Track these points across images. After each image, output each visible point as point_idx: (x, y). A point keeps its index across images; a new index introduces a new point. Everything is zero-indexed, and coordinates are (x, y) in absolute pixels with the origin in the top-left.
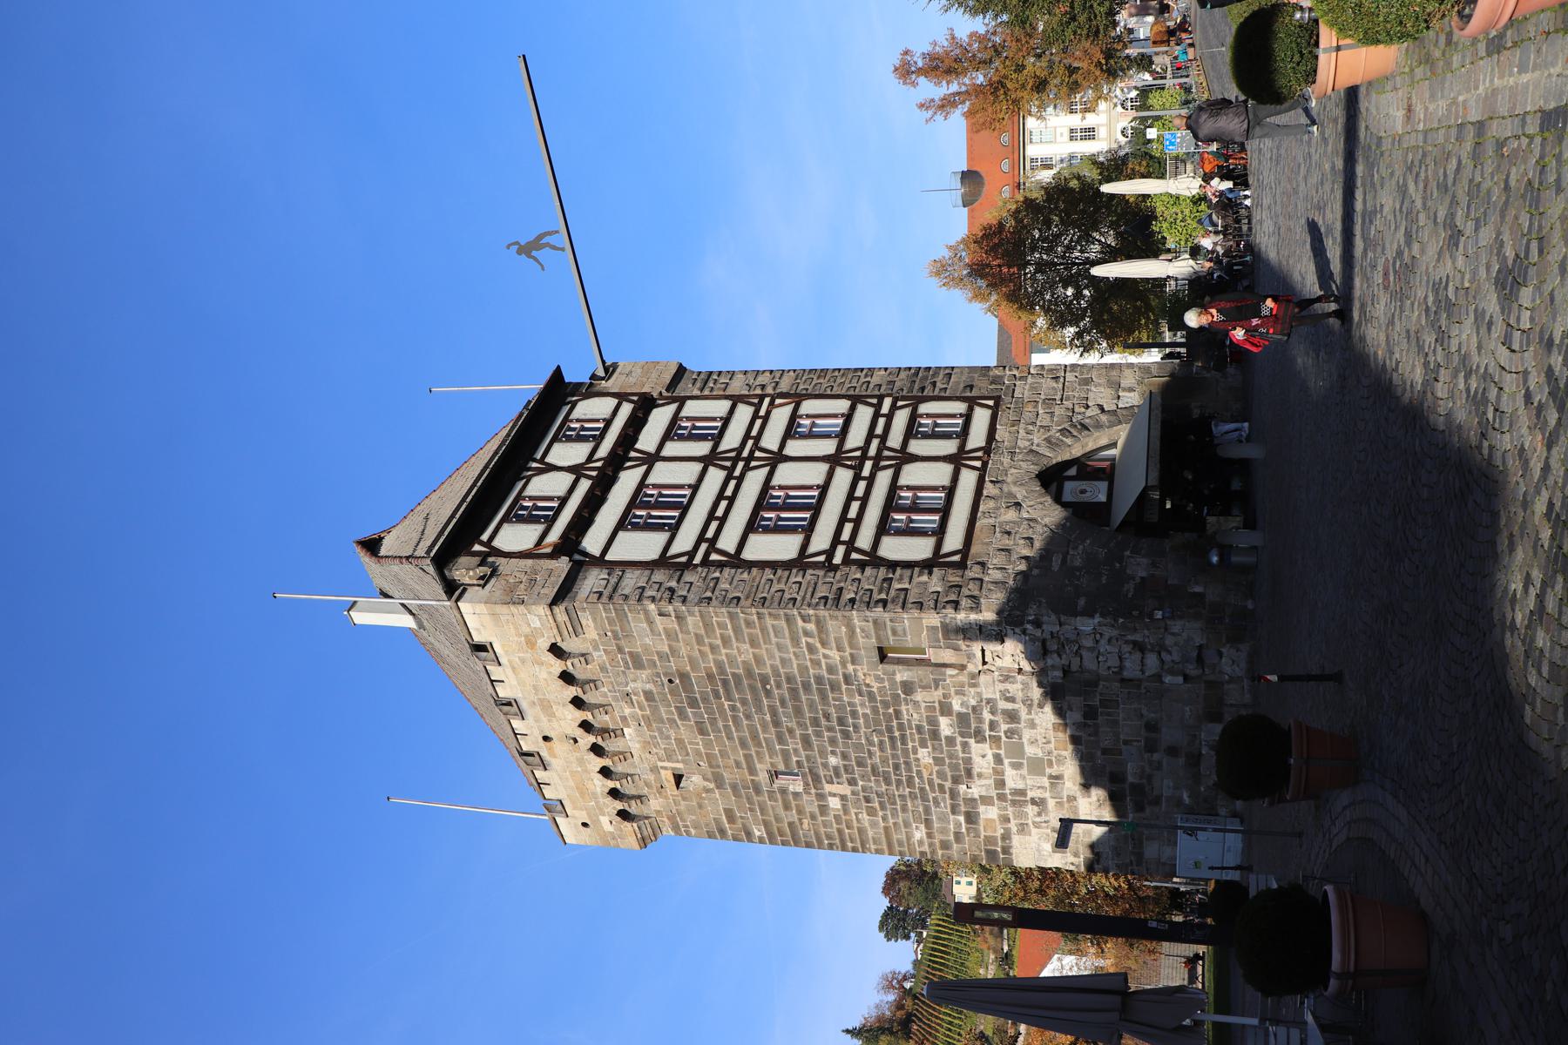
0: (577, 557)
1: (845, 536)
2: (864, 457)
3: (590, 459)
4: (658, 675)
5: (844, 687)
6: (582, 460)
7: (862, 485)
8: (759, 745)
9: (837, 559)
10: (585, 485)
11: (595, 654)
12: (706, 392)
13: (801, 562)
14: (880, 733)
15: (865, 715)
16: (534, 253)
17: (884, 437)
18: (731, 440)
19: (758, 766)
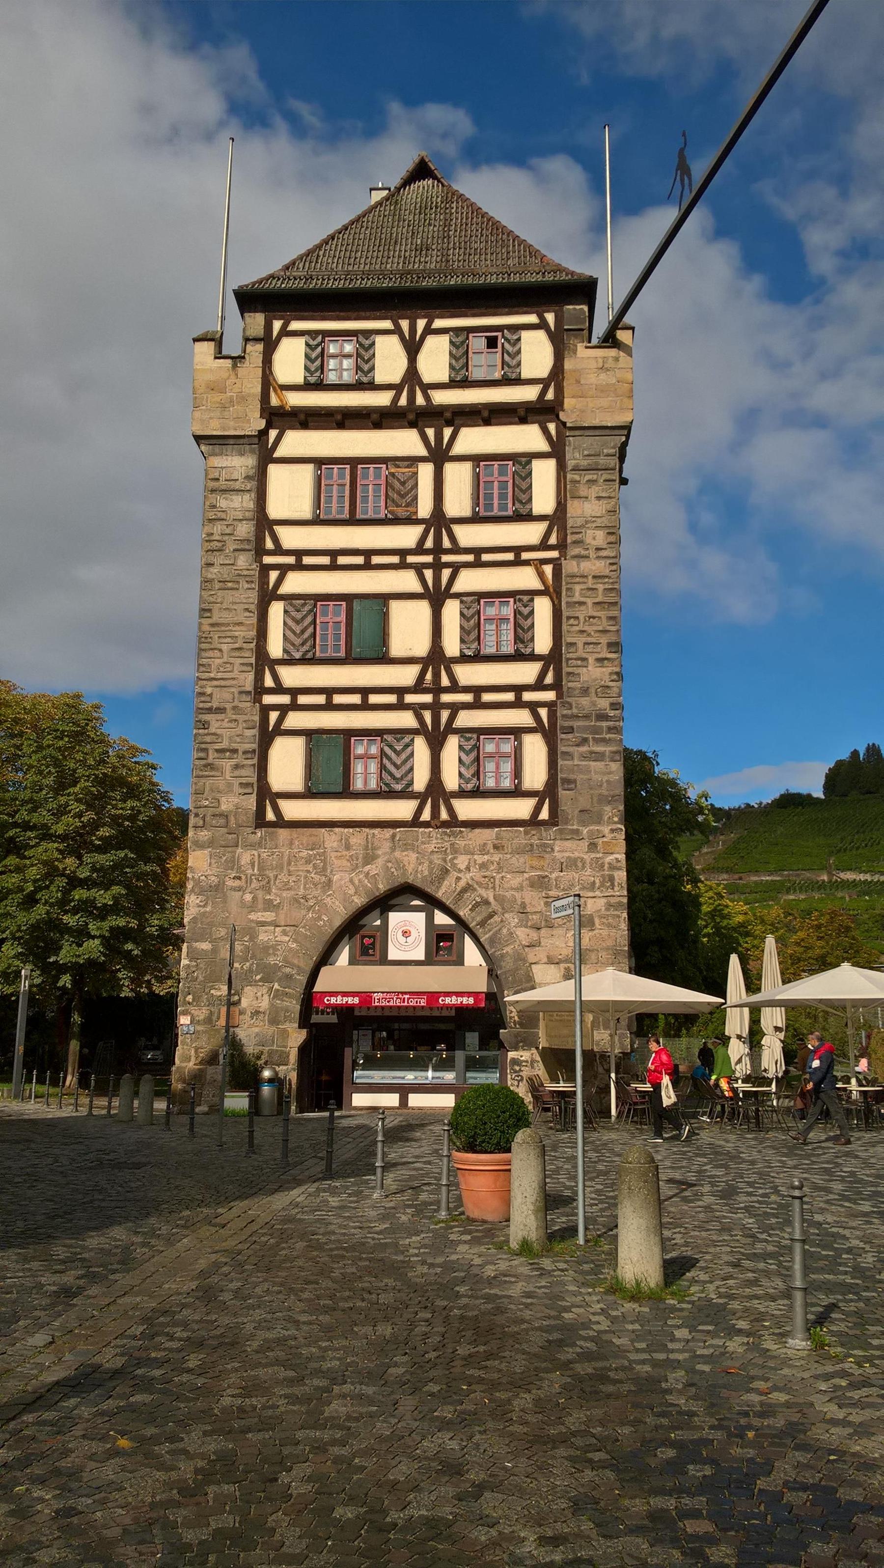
3: (427, 388)
6: (427, 378)
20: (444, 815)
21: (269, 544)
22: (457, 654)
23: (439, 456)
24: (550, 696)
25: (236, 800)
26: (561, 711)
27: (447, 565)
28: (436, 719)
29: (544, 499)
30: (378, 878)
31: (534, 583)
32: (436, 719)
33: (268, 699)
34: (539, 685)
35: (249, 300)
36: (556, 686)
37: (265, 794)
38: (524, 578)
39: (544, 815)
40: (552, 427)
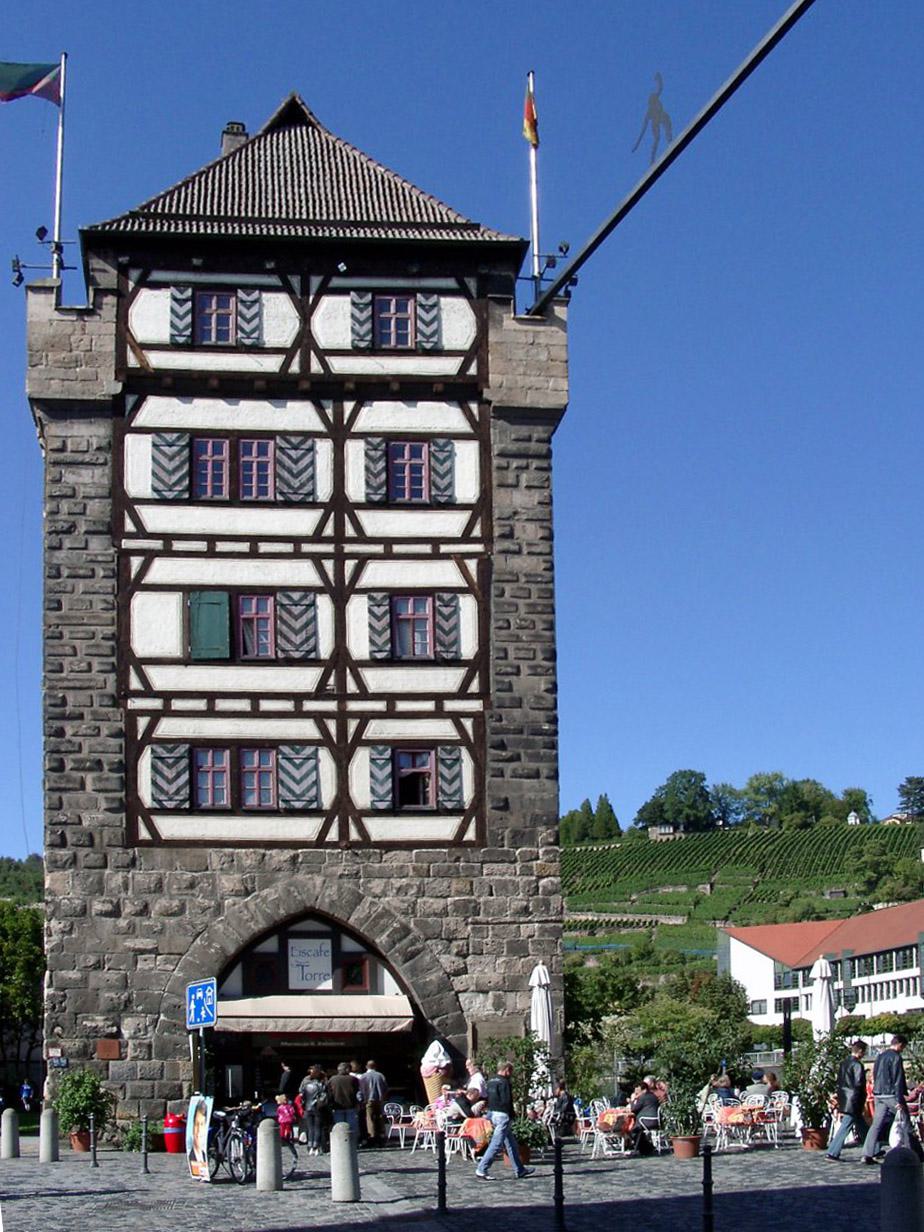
3: (323, 354)
6: (323, 342)
20: (354, 835)
21: (129, 526)
22: (366, 656)
23: (339, 433)
24: (476, 705)
25: (101, 816)
26: (491, 724)
27: (352, 556)
28: (342, 729)
29: (467, 487)
30: (272, 900)
31: (457, 580)
32: (342, 729)
33: (135, 704)
34: (462, 694)
35: (96, 242)
36: (483, 694)
37: (130, 806)
38: (444, 574)
39: (470, 835)
40: (474, 407)
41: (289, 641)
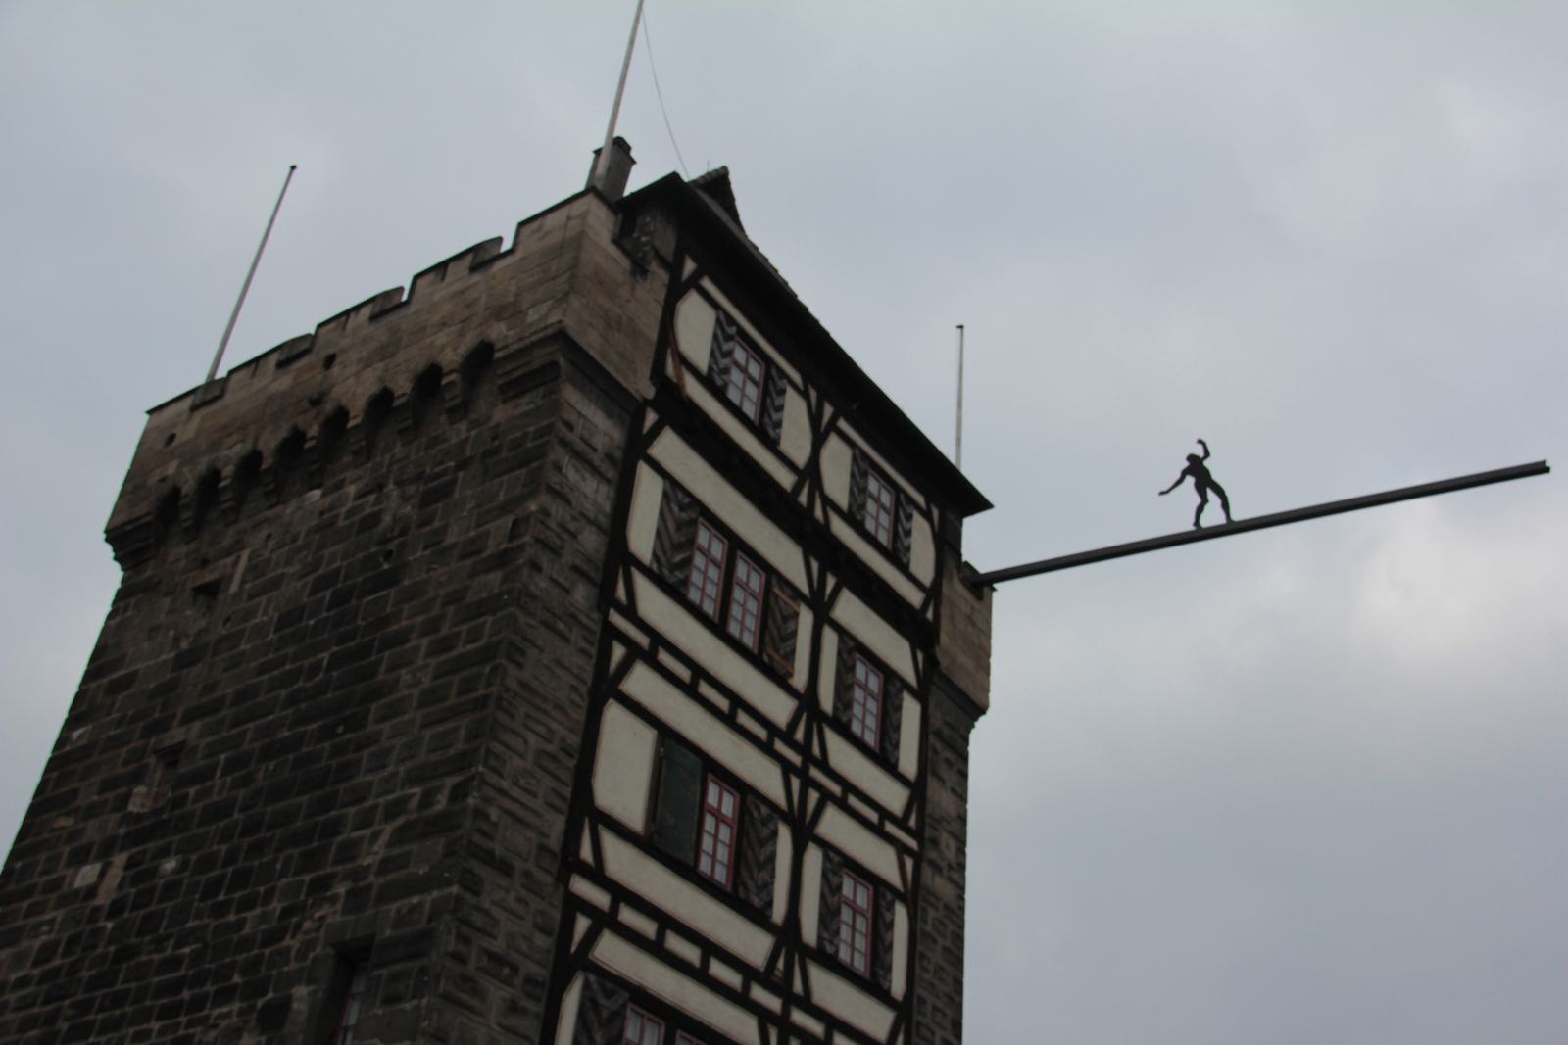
0: (651, 418)
1: (628, 916)
2: (790, 999)
4: (404, 532)
5: (307, 878)
7: (731, 978)
8: (236, 723)
9: (582, 887)
10: (786, 479)
11: (463, 426)
12: (932, 739)
13: (584, 811)
14: (197, 958)
15: (240, 925)
16: (1190, 480)
17: (884, 813)
18: (844, 758)
19: (197, 725)
40: (920, 656)
41: (751, 877)
